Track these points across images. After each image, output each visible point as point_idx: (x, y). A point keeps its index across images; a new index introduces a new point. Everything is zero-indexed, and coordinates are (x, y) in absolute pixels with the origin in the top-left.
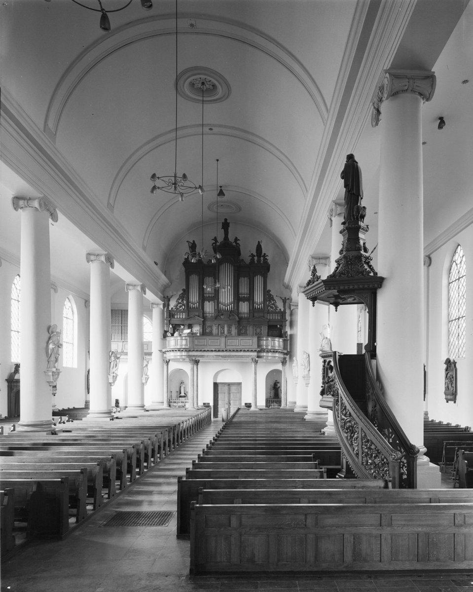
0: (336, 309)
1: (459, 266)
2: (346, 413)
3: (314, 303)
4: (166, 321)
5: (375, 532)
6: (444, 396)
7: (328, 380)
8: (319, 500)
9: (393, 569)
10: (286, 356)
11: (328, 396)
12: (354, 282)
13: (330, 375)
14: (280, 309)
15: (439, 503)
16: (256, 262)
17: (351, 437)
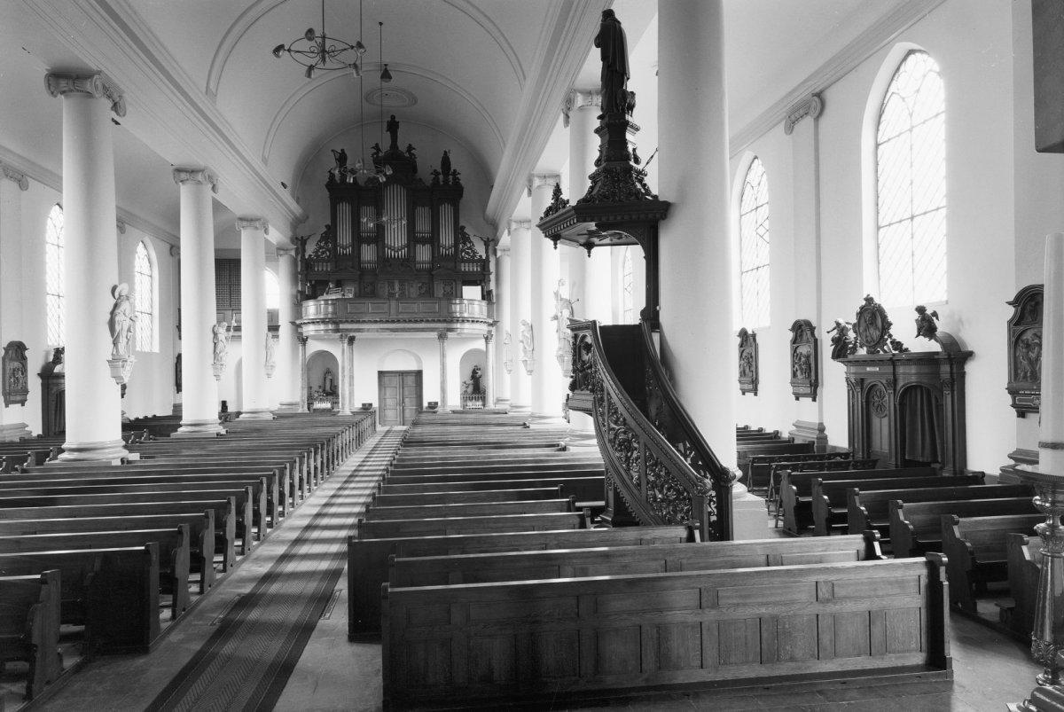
0: (589, 253)
1: (756, 189)
2: (618, 419)
3: (555, 244)
4: (300, 276)
5: (692, 618)
6: (791, 389)
7: (582, 366)
8: (520, 548)
9: (721, 679)
10: (491, 328)
11: (583, 392)
12: (618, 207)
13: (586, 358)
14: (481, 256)
15: (782, 565)
16: (442, 183)
17: (628, 459)
